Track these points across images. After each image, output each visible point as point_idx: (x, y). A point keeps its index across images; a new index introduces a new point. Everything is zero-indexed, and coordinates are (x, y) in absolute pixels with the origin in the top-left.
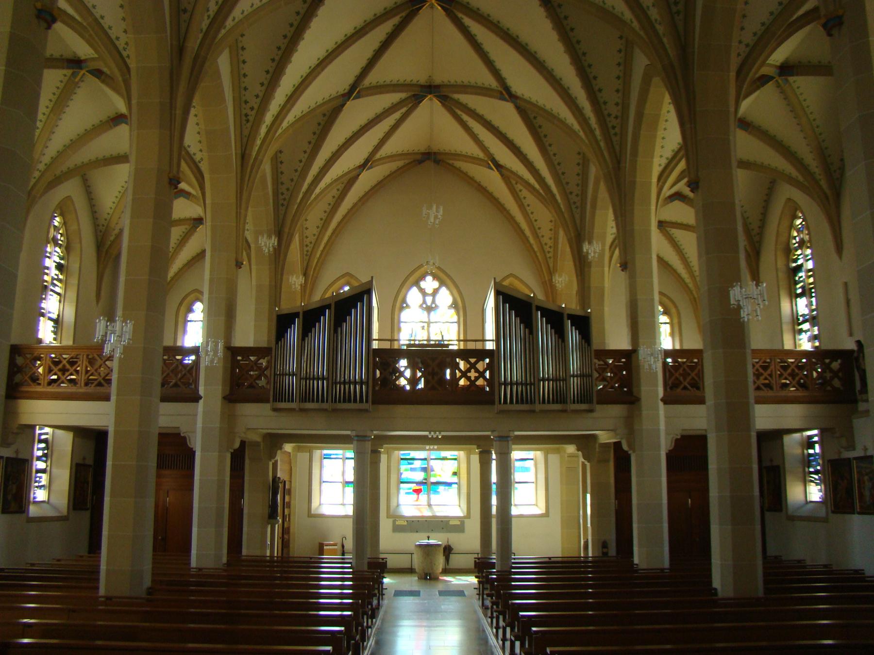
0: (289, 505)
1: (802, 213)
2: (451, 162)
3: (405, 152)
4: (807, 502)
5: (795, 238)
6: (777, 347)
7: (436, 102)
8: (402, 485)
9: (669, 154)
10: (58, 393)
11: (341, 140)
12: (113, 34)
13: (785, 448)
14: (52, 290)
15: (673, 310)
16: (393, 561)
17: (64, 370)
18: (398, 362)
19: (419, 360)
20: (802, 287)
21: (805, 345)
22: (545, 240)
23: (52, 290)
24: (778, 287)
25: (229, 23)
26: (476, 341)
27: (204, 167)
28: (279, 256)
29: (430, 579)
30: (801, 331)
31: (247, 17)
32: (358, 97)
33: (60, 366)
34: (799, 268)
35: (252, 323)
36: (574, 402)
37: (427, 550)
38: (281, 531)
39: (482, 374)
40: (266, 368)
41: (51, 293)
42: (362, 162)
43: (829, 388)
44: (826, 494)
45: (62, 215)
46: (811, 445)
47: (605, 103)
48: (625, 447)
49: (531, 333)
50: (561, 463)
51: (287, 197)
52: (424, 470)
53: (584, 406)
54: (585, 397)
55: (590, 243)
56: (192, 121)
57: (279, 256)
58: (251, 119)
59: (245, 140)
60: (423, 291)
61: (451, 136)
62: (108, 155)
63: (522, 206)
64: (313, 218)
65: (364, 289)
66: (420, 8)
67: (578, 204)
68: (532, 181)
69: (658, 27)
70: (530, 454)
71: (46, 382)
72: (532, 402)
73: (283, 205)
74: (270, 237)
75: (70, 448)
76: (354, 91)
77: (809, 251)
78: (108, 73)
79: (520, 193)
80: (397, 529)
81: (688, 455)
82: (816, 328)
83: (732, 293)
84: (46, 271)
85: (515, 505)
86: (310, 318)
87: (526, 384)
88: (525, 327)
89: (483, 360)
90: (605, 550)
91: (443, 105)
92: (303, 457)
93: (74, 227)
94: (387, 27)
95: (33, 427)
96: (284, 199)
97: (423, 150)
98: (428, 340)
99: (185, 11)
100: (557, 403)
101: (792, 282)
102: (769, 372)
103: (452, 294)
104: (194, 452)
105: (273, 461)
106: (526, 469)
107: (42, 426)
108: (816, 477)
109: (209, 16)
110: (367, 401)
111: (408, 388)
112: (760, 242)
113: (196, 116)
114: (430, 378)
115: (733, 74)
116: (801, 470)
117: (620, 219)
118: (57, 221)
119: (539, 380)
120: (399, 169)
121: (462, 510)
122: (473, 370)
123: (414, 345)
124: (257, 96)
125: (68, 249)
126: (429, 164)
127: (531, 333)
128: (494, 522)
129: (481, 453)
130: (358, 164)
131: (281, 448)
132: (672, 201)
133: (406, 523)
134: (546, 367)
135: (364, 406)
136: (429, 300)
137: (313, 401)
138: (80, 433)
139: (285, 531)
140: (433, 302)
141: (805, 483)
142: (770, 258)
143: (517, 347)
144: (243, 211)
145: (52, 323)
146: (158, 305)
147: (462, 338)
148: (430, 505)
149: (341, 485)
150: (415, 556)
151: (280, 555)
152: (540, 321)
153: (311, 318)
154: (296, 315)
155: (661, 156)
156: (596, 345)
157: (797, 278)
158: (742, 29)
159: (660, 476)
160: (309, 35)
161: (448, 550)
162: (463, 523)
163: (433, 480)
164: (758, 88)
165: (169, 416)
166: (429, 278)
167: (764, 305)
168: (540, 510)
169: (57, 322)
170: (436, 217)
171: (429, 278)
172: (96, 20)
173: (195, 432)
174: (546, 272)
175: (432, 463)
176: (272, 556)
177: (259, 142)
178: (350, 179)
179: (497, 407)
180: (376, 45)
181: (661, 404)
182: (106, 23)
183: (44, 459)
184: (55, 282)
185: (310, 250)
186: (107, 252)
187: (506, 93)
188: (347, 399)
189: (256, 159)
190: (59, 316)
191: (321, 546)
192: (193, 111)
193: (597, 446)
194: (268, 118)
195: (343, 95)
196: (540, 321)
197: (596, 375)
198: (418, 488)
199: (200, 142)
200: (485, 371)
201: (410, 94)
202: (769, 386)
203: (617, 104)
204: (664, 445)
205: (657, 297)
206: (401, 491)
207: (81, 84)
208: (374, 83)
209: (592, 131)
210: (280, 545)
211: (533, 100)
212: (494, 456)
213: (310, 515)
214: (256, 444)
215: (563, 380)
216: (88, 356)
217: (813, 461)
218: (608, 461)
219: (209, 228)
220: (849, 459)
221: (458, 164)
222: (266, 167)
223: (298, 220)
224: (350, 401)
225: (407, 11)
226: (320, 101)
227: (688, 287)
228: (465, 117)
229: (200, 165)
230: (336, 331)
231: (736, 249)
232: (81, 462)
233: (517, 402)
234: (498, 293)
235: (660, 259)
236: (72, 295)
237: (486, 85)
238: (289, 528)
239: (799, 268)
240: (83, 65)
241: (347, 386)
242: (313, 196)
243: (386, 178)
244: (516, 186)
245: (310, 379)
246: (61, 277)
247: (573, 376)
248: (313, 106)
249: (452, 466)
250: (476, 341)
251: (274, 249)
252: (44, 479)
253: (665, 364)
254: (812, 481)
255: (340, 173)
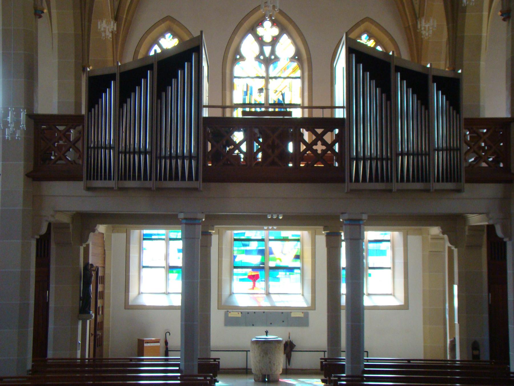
0: (102, 295)
8: (235, 271)
16: (226, 360)
19: (256, 131)
29: (269, 381)
36: (438, 181)
37: (266, 346)
38: (93, 326)
39: (330, 147)
40: (77, 140)
48: (499, 233)
49: (389, 98)
52: (261, 252)
53: (450, 186)
54: (451, 174)
60: (259, 39)
65: (193, 45)
70: (387, 235)
72: (389, 180)
80: (230, 322)
85: (369, 295)
86: (129, 80)
87: (382, 159)
88: (382, 92)
90: (476, 353)
92: (117, 238)
100: (418, 181)
103: (295, 43)
105: (84, 245)
106: (382, 253)
110: (197, 179)
119: (397, 155)
121: (306, 301)
122: (319, 143)
127: (389, 98)
128: (343, 314)
129: (328, 235)
131: (94, 231)
133: (240, 315)
134: (406, 134)
136: (267, 50)
137: (134, 179)
139: (98, 326)
140: (273, 52)
148: (268, 294)
149: (163, 270)
150: (250, 354)
151: (92, 356)
154: (112, 77)
156: (466, 114)
161: (289, 347)
162: (306, 315)
163: (272, 264)
168: (398, 301)
175: (271, 244)
176: (83, 358)
179: (347, 186)
191: (141, 343)
197: (465, 148)
198: (254, 273)
200: (333, 144)
206: (235, 277)
210: (92, 344)
213: (127, 306)
215: (426, 155)
218: (480, 246)
224: (177, 178)
230: (159, 97)
233: (371, 180)
234: (350, 51)
238: (102, 323)
241: (173, 162)
247: (438, 150)
249: (293, 248)
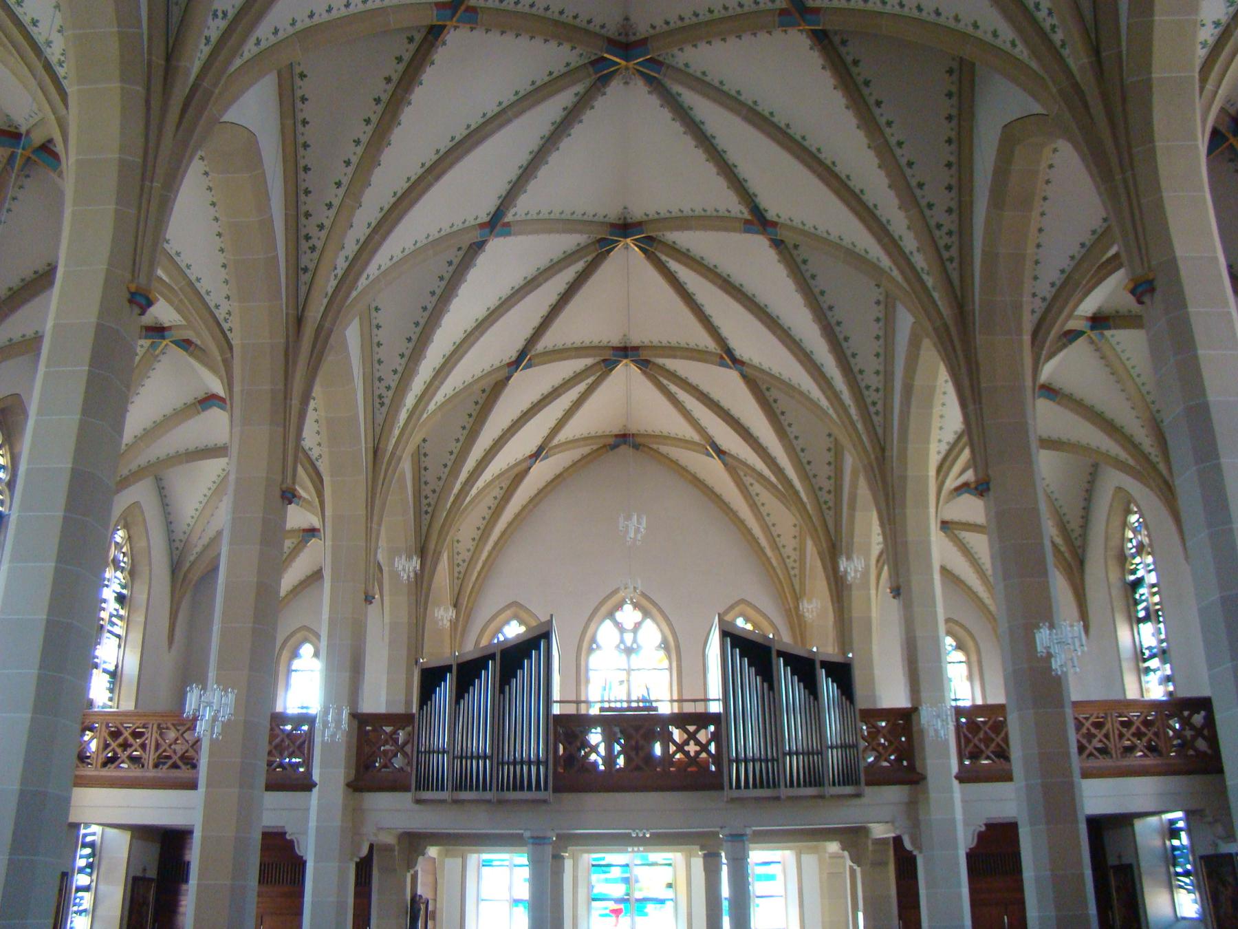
1: (1138, 507)
2: (655, 447)
3: (593, 434)
4: (1178, 919)
5: (1130, 540)
6: (1114, 696)
7: (633, 368)
8: (594, 904)
9: (951, 438)
10: (116, 778)
11: (505, 423)
12: (211, 301)
13: (1138, 838)
14: (109, 632)
15: (970, 644)
17: (125, 746)
18: (587, 732)
19: (617, 730)
20: (1146, 609)
21: (1156, 691)
22: (788, 551)
23: (109, 632)
24: (1113, 609)
25: (363, 282)
26: (694, 701)
27: (323, 466)
28: (421, 585)
30: (1147, 670)
31: (385, 273)
32: (528, 366)
33: (121, 740)
34: (1139, 582)
35: (385, 678)
36: (834, 784)
39: (704, 748)
41: (108, 635)
42: (535, 449)
43: (1191, 752)
44: (1202, 906)
45: (126, 526)
46: (1174, 833)
47: (861, 372)
48: (908, 845)
49: (771, 688)
50: (820, 869)
51: (433, 503)
52: (626, 880)
53: (849, 790)
54: (849, 776)
55: (849, 558)
56: (311, 416)
57: (421, 585)
58: (387, 401)
59: (378, 430)
60: (618, 625)
61: (652, 411)
62: (192, 448)
63: (753, 506)
64: (465, 530)
66: (609, 251)
67: (831, 504)
68: (767, 472)
69: (925, 277)
71: (100, 761)
72: (775, 785)
73: (427, 512)
74: (409, 558)
75: (126, 855)
76: (522, 359)
77: (1149, 559)
78: (199, 343)
79: (750, 489)
81: (995, 853)
82: (1168, 666)
83: (1038, 636)
84: (103, 605)
87: (767, 761)
88: (763, 681)
89: (706, 728)
91: (644, 373)
92: (452, 863)
93: (141, 544)
94: (569, 274)
95: (76, 826)
96: (429, 505)
97: (616, 431)
98: (629, 701)
99: (305, 270)
101: (1131, 602)
102: (1104, 731)
104: (305, 862)
105: (412, 872)
106: (771, 877)
107: (87, 825)
108: (1187, 880)
109: (336, 276)
110: (546, 789)
111: (602, 768)
112: (1084, 547)
113: (315, 410)
114: (633, 754)
115: (1027, 338)
116: (1163, 870)
117: (887, 527)
118: (120, 536)
119: (785, 754)
120: (584, 457)
122: (692, 742)
123: (610, 709)
124: (395, 372)
125: (132, 573)
126: (623, 449)
127: (771, 688)
129: (705, 856)
130: (528, 453)
132: (959, 495)
134: (794, 732)
135: (541, 795)
137: (471, 789)
138: (141, 833)
140: (635, 641)
141: (1171, 889)
142: (1098, 570)
143: (751, 702)
144: (375, 526)
145: (107, 677)
146: (262, 667)
147: (675, 697)
149: (507, 904)
152: (783, 673)
153: (468, 672)
154: (448, 668)
155: (940, 441)
156: (862, 703)
157: (1137, 596)
158: (1036, 278)
159: (959, 885)
160: (464, 290)
163: (638, 895)
164: (1064, 346)
165: (276, 810)
166: (628, 608)
167: (1083, 652)
169: (114, 675)
170: (637, 530)
171: (628, 608)
172: (191, 284)
173: (305, 833)
174: (790, 597)
177: (397, 432)
178: (518, 475)
179: (727, 793)
180: (553, 298)
181: (956, 782)
182: (202, 287)
183: (88, 870)
184: (114, 619)
185: (463, 571)
186: (185, 576)
187: (729, 358)
188: (518, 786)
189: (393, 454)
190: (117, 666)
192: (312, 404)
193: (870, 842)
194: (410, 400)
195: (509, 365)
196: (783, 673)
197: (863, 744)
199: (318, 433)
200: (709, 743)
201: (598, 359)
202: (1104, 751)
203: (877, 373)
204: (964, 841)
205: (942, 628)
207: (162, 357)
208: (550, 347)
209: (845, 409)
211: (765, 366)
212: (724, 860)
214: (387, 848)
216: (159, 725)
217: (1180, 856)
219: (329, 543)
220: (1231, 855)
221: (664, 449)
222: (406, 466)
223: (447, 533)
224: (522, 788)
225: (594, 255)
226: (478, 374)
227: (988, 610)
228: (673, 388)
229: (318, 464)
230: (502, 691)
231: (1043, 565)
232: (139, 874)
233: (755, 786)
234: (724, 634)
235: (944, 570)
236: (136, 637)
237: (702, 347)
239: (1139, 582)
240: (166, 333)
242: (468, 499)
243: (566, 469)
244: (744, 479)
245: (466, 758)
246: (122, 612)
248: (469, 380)
249: (666, 875)
250: (694, 701)
251: (416, 574)
252: (87, 900)
253: (958, 726)
254: (1181, 887)
255: (504, 467)
